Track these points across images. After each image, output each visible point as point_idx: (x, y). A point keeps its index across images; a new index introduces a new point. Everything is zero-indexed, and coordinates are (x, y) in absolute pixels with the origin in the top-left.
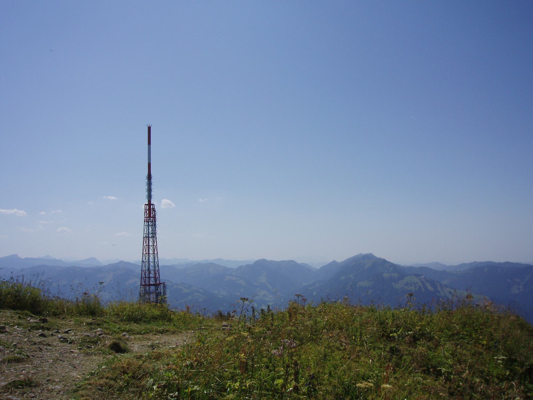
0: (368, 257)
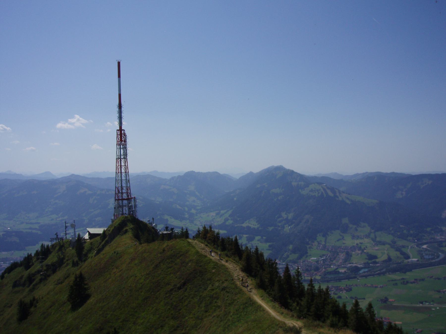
0: (280, 168)
